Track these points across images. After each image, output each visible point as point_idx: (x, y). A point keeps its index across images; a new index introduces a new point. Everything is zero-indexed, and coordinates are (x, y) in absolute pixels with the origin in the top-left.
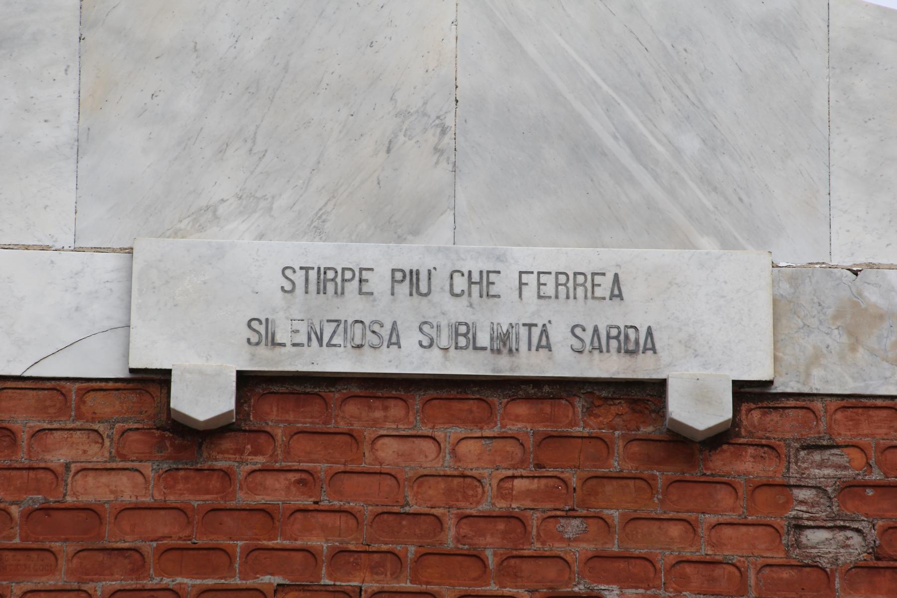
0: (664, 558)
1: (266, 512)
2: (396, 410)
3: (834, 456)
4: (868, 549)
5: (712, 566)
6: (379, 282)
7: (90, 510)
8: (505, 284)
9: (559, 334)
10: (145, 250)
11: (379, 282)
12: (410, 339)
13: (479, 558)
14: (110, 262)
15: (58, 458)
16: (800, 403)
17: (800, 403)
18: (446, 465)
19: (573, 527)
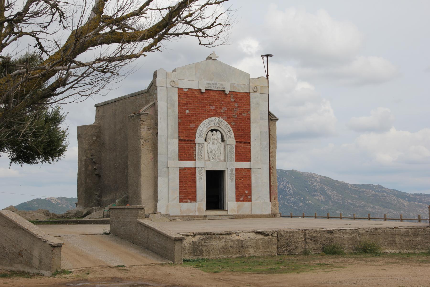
0: (225, 101)
1: (206, 97)
2: (212, 91)
3: (233, 95)
4: (37, 107)
5: (216, 215)
6: (211, 84)
7: (198, 97)
8: (217, 84)
9: (220, 87)
10: (200, 81)
11: (211, 84)
12: (213, 88)
13: (216, 100)
14: (198, 82)
15: (196, 94)
16: (122, 268)
17: (122, 268)
18: (214, 95)
19: (220, 99)
